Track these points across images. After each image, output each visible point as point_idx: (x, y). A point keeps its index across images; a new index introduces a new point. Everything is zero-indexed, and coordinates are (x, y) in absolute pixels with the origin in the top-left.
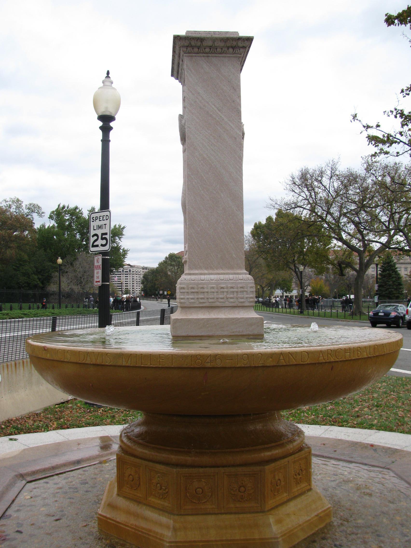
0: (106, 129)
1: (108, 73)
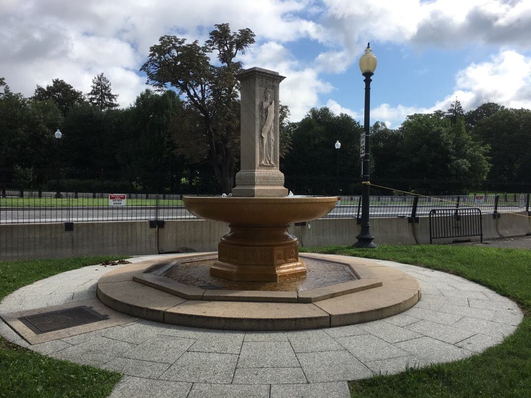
0: (368, 81)
1: (369, 44)
